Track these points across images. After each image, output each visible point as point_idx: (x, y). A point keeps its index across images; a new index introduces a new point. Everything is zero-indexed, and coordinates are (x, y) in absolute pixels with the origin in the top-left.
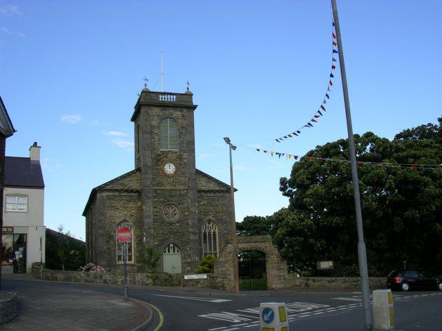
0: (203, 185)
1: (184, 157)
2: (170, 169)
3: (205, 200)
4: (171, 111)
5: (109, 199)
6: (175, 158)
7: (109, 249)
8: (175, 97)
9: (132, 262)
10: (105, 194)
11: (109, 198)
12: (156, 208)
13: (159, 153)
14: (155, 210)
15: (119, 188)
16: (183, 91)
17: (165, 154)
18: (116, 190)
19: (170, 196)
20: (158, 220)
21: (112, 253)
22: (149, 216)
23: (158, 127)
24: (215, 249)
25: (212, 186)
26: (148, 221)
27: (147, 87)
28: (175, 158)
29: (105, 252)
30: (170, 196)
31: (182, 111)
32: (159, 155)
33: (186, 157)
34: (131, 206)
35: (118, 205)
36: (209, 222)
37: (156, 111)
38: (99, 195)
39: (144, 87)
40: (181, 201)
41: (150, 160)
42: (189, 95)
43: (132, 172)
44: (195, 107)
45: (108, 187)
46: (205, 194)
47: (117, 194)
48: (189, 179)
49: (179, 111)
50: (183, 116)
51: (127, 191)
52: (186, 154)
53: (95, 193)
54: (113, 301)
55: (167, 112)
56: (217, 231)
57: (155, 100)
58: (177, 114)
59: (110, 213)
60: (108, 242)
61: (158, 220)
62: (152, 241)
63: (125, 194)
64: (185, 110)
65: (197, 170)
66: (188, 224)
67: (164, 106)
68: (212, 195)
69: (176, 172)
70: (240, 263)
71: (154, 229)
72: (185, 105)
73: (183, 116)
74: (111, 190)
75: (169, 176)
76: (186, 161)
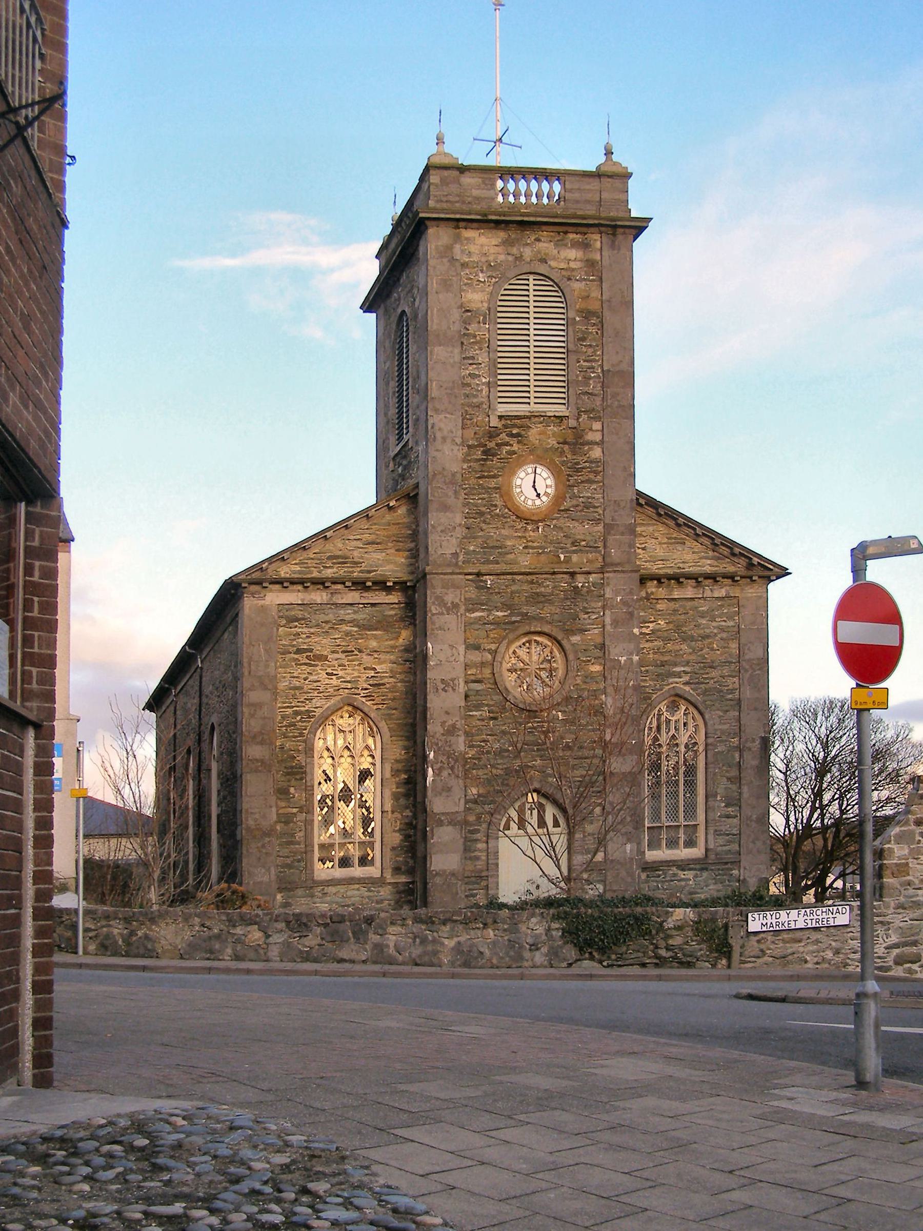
0: (657, 551)
1: (590, 436)
2: (533, 486)
3: (660, 614)
4: (546, 246)
5: (292, 620)
6: (552, 442)
7: (287, 819)
8: (557, 187)
9: (373, 871)
10: (275, 598)
11: (290, 617)
12: (477, 648)
13: (494, 422)
14: (475, 657)
15: (329, 573)
16: (591, 162)
17: (516, 426)
18: (320, 583)
19: (536, 599)
20: (486, 691)
21: (299, 836)
22: (448, 685)
23: (489, 315)
24: (691, 810)
25: (691, 557)
26: (443, 705)
27: (448, 148)
28: (552, 442)
29: (270, 833)
30: (536, 599)
31: (585, 246)
32: (492, 434)
33: (597, 437)
34: (374, 644)
35: (322, 644)
36: (676, 699)
37: (483, 244)
38: (249, 604)
39: (434, 149)
40: (575, 617)
41: (460, 453)
42: (613, 177)
43: (365, 514)
44: (639, 227)
45: (284, 571)
46: (662, 592)
47: (319, 596)
48: (608, 528)
49: (575, 245)
50: (591, 264)
51: (360, 585)
52: (597, 426)
53: (229, 597)
54: (191, 782)
55: (528, 253)
56: (701, 738)
57: (478, 199)
58: (567, 256)
59: (289, 676)
60: (283, 792)
61: (486, 691)
62: (457, 785)
63: (353, 596)
64: (596, 239)
65: (639, 494)
66: (599, 711)
67: (517, 224)
68: (689, 591)
69: (558, 499)
70: (13, 596)
71: (467, 734)
72: (594, 220)
73: (591, 264)
74: (301, 582)
75: (526, 519)
76: (596, 453)
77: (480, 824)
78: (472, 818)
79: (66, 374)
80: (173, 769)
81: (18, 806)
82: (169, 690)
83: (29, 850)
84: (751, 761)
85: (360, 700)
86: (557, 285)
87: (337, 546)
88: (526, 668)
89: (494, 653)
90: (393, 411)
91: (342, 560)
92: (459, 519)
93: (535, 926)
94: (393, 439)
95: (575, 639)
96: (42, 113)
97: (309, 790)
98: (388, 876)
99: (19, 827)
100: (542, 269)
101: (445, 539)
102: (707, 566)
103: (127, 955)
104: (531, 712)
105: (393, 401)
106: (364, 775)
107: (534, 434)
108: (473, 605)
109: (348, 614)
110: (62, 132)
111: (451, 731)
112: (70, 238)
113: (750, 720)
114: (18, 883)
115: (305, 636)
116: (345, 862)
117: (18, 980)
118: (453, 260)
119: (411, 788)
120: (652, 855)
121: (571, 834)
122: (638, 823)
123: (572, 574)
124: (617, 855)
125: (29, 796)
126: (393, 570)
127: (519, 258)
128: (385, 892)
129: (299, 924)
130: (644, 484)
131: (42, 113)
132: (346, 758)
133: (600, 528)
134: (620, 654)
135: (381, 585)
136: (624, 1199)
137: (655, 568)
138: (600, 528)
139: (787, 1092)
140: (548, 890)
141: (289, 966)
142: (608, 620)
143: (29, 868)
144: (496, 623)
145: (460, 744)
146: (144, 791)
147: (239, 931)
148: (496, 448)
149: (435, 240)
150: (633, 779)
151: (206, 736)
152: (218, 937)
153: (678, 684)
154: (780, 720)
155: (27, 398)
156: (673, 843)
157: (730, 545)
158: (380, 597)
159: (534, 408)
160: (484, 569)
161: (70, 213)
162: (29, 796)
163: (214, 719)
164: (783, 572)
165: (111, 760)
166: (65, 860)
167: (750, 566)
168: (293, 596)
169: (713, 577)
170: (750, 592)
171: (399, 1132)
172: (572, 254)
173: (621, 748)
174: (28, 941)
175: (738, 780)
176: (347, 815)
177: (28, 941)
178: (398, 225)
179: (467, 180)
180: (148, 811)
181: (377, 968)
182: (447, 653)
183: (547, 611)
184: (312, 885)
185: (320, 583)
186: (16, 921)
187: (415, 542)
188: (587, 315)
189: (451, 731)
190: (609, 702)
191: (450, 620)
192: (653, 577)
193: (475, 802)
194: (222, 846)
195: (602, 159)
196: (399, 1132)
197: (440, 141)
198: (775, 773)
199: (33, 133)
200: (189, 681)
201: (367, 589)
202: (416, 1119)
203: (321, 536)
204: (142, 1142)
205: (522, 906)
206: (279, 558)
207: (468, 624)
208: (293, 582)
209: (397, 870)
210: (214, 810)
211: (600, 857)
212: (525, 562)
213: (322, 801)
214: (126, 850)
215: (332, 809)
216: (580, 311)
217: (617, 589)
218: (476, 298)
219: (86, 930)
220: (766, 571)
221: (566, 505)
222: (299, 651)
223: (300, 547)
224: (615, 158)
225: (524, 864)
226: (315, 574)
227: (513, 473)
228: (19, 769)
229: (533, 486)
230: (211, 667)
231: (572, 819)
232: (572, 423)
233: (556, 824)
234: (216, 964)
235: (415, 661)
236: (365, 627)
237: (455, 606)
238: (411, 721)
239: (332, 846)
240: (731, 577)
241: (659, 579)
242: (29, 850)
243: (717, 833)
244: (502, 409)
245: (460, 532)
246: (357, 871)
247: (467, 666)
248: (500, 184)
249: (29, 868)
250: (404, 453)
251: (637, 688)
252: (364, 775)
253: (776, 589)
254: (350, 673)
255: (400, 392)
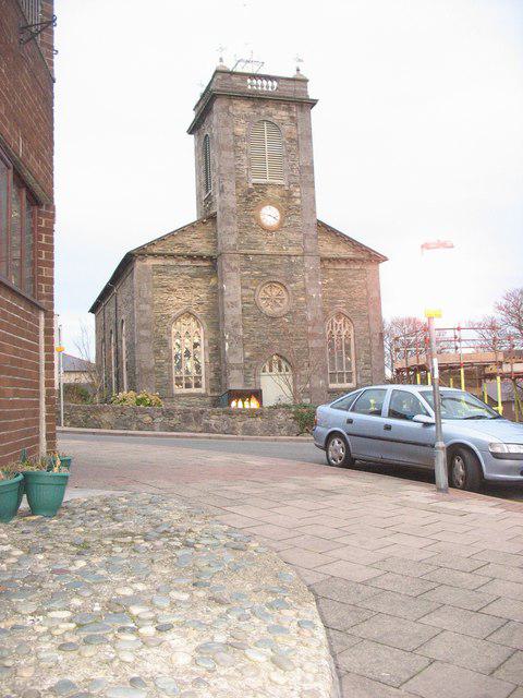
0: (329, 248)
2: (270, 216)
4: (271, 109)
9: (202, 390)
10: (150, 262)
11: (159, 271)
13: (251, 186)
14: (245, 292)
17: (261, 188)
18: (172, 256)
20: (251, 310)
22: (234, 304)
25: (343, 251)
26: (233, 313)
32: (250, 191)
34: (198, 285)
35: (174, 283)
36: (339, 315)
37: (243, 107)
38: (138, 264)
39: (219, 64)
43: (192, 225)
44: (313, 103)
46: (331, 266)
47: (171, 262)
51: (190, 257)
52: (298, 190)
53: (128, 262)
58: (281, 114)
60: (157, 352)
61: (251, 310)
63: (188, 263)
66: (304, 319)
67: (258, 99)
68: (343, 266)
69: (281, 223)
73: (292, 118)
75: (268, 230)
76: (298, 202)
77: (250, 369)
78: (247, 367)
79: (56, 148)
80: (104, 341)
81: (37, 349)
82: (112, 288)
83: (43, 371)
84: (375, 344)
85: (193, 310)
86: (275, 126)
87: (179, 240)
88: (273, 301)
89: (255, 290)
90: (203, 179)
91: (182, 245)
92: (236, 229)
93: (281, 417)
94: (204, 192)
95: (292, 285)
96: (42, 30)
97: (170, 351)
98: (209, 394)
99: (38, 358)
100: (269, 119)
101: (229, 235)
102: (350, 254)
103: (86, 427)
104: (273, 318)
105: (203, 175)
106: (196, 345)
107: (269, 192)
108: (244, 268)
109: (186, 271)
110: (52, 39)
111: (236, 326)
112: (56, 86)
113: (373, 325)
114: (37, 386)
115: (166, 279)
116: (188, 386)
117: (39, 432)
118: (229, 113)
119: (216, 351)
120: (332, 386)
121: (294, 374)
122: (325, 371)
123: (289, 256)
124: (315, 385)
125: (42, 345)
126: (200, 253)
127: (259, 114)
128: (207, 400)
129: (169, 413)
130: (322, 216)
131: (42, 30)
132: (188, 338)
133: (302, 235)
134: (314, 293)
135: (200, 257)
136: (318, 570)
137: (326, 255)
138: (302, 235)
139: (405, 493)
140: (289, 402)
141: (164, 433)
142: (307, 277)
143: (43, 379)
144: (255, 277)
145: (240, 332)
146: (90, 354)
147: (140, 416)
148: (252, 197)
149: (217, 106)
150: (322, 351)
151: (119, 325)
152: (130, 419)
153: (341, 308)
154: (387, 327)
155: (38, 157)
156: (341, 381)
157: (361, 245)
158: (201, 264)
159: (268, 180)
160: (249, 251)
161: (56, 75)
162: (42, 345)
163: (123, 317)
164: (386, 259)
165: (75, 333)
166: (60, 379)
167: (371, 256)
168: (160, 262)
169: (353, 260)
170: (370, 268)
171: (228, 508)
172: (284, 113)
173: (314, 335)
174: (43, 414)
175: (369, 352)
176: (189, 364)
177: (43, 414)
178: (203, 95)
179: (233, 78)
180: (93, 361)
181: (206, 435)
182: (233, 288)
183: (278, 272)
184: (173, 397)
185: (172, 256)
186: (37, 404)
187: (214, 239)
188: (291, 140)
189: (236, 326)
190: (310, 316)
191: (234, 275)
192: (326, 259)
193: (248, 359)
194: (129, 377)
195: (296, 73)
196: (228, 508)
197: (221, 60)
198: (386, 350)
199: (39, 39)
200: (110, 299)
201: (195, 259)
202: (233, 502)
203: (172, 235)
204: (107, 509)
205: (275, 407)
206: (152, 244)
207: (242, 277)
208: (159, 255)
209: (213, 390)
210: (125, 360)
211: (308, 386)
212: (267, 250)
213: (176, 357)
214: (84, 379)
215: (181, 360)
216: (288, 139)
217: (311, 264)
218: (240, 130)
219: (65, 415)
220: (375, 258)
221: (285, 224)
222: (163, 287)
223: (162, 239)
224: (301, 72)
225: (275, 387)
226: (169, 251)
227: (260, 209)
228: (37, 331)
229: (270, 216)
230: (122, 293)
231: (293, 367)
232: (287, 188)
233: (287, 370)
234: (130, 432)
235: (217, 293)
236: (193, 277)
237: (235, 268)
238: (215, 318)
239: (181, 378)
240: (361, 260)
241: (329, 260)
242: (43, 371)
243: (362, 377)
244: (254, 181)
245: (236, 235)
246: (194, 390)
247: (242, 296)
248: (249, 81)
249: (43, 379)
250: (209, 198)
251: (322, 309)
252: (196, 345)
253: (382, 266)
254: (188, 298)
255: (207, 170)
